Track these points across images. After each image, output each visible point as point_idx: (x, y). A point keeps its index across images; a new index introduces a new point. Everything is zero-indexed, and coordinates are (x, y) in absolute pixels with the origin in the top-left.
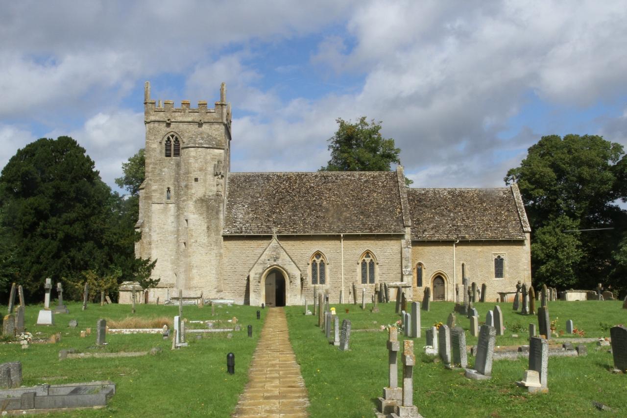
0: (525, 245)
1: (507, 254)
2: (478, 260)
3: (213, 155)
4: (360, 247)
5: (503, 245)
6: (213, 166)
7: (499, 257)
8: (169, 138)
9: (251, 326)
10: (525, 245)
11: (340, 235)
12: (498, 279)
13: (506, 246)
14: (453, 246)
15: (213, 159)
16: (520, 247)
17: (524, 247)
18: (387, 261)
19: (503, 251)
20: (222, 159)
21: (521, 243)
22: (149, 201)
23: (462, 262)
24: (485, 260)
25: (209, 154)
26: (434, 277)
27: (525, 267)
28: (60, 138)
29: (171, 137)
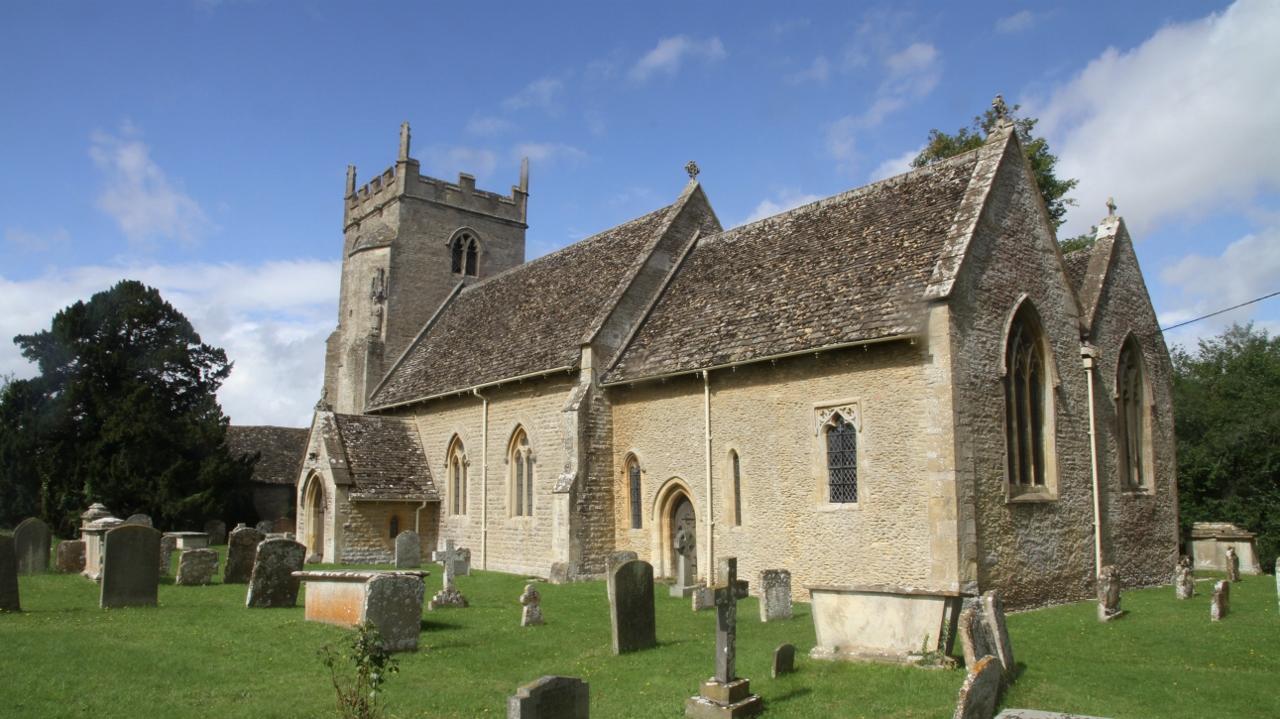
0: (929, 359)
1: (864, 404)
2: (772, 437)
3: (373, 262)
4: (809, 401)
5: (849, 370)
6: (370, 282)
7: (837, 417)
8: (459, 240)
9: (768, 572)
10: (929, 359)
11: (472, 391)
12: (838, 506)
13: (860, 374)
14: (703, 392)
15: (371, 270)
16: (911, 370)
17: (928, 370)
18: (548, 453)
19: (851, 392)
20: (386, 265)
21: (906, 350)
22: (334, 364)
23: (728, 447)
24: (794, 433)
25: (366, 261)
26: (668, 507)
27: (933, 455)
28: (96, 298)
29: (462, 239)
